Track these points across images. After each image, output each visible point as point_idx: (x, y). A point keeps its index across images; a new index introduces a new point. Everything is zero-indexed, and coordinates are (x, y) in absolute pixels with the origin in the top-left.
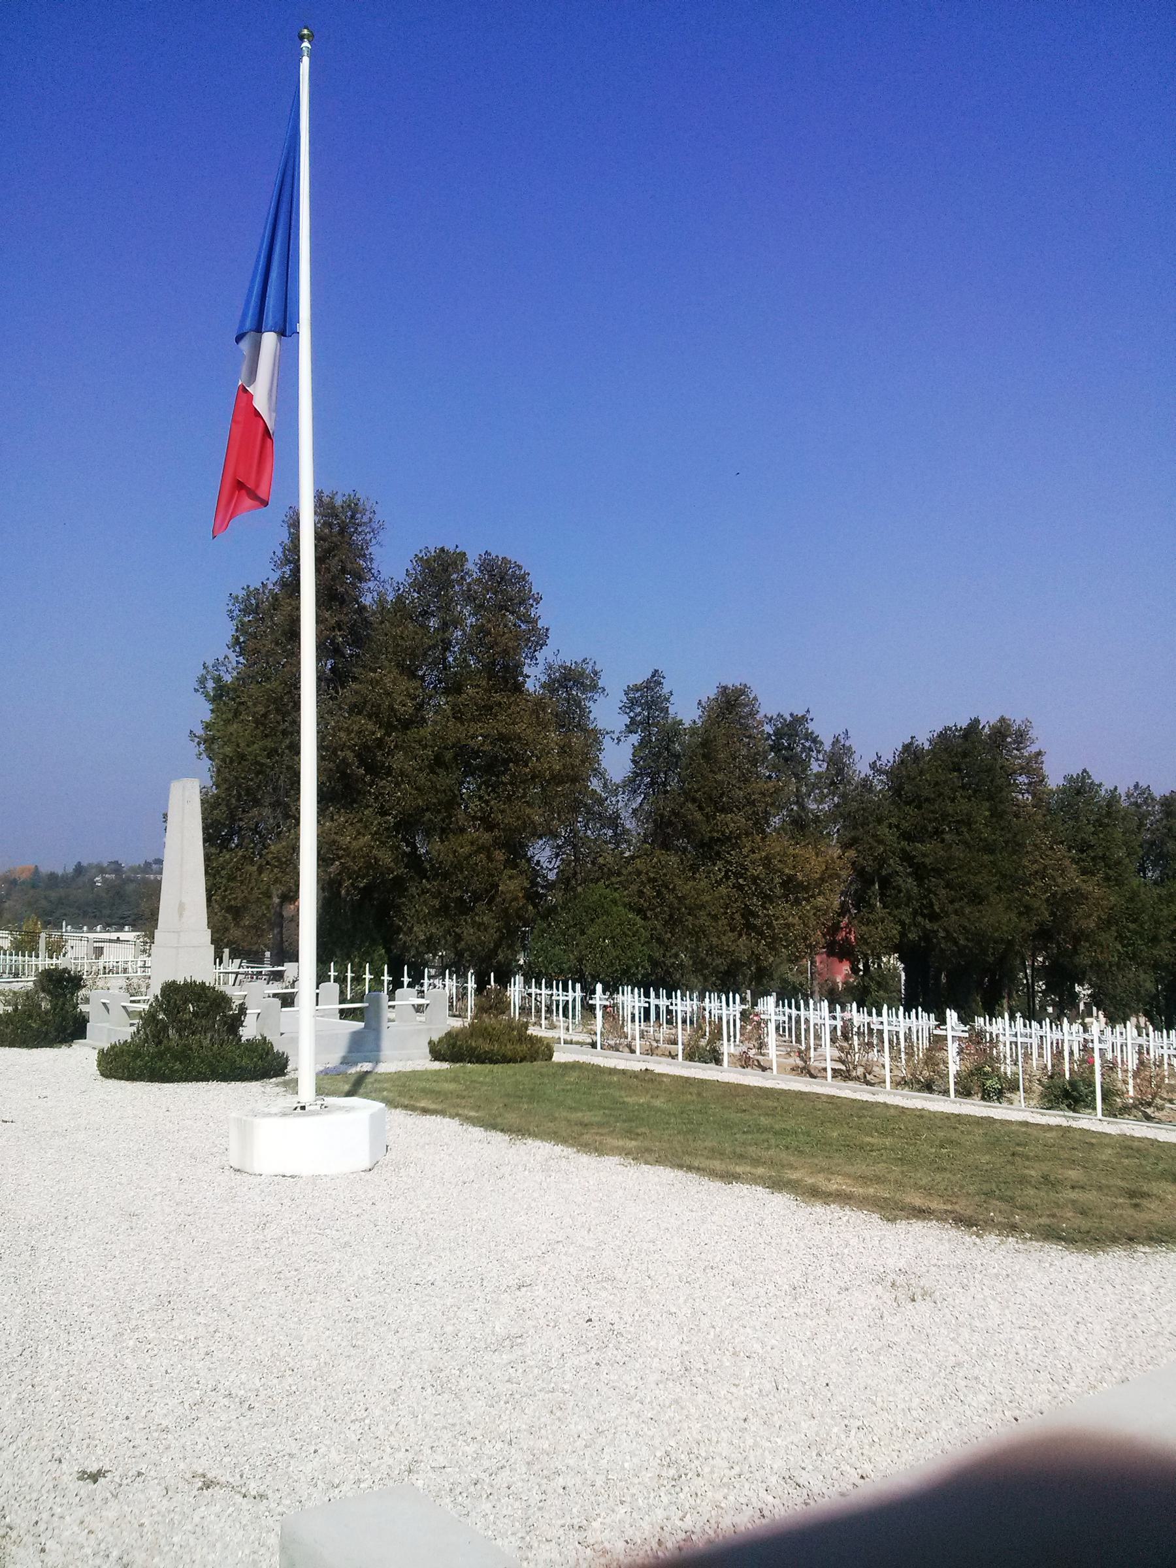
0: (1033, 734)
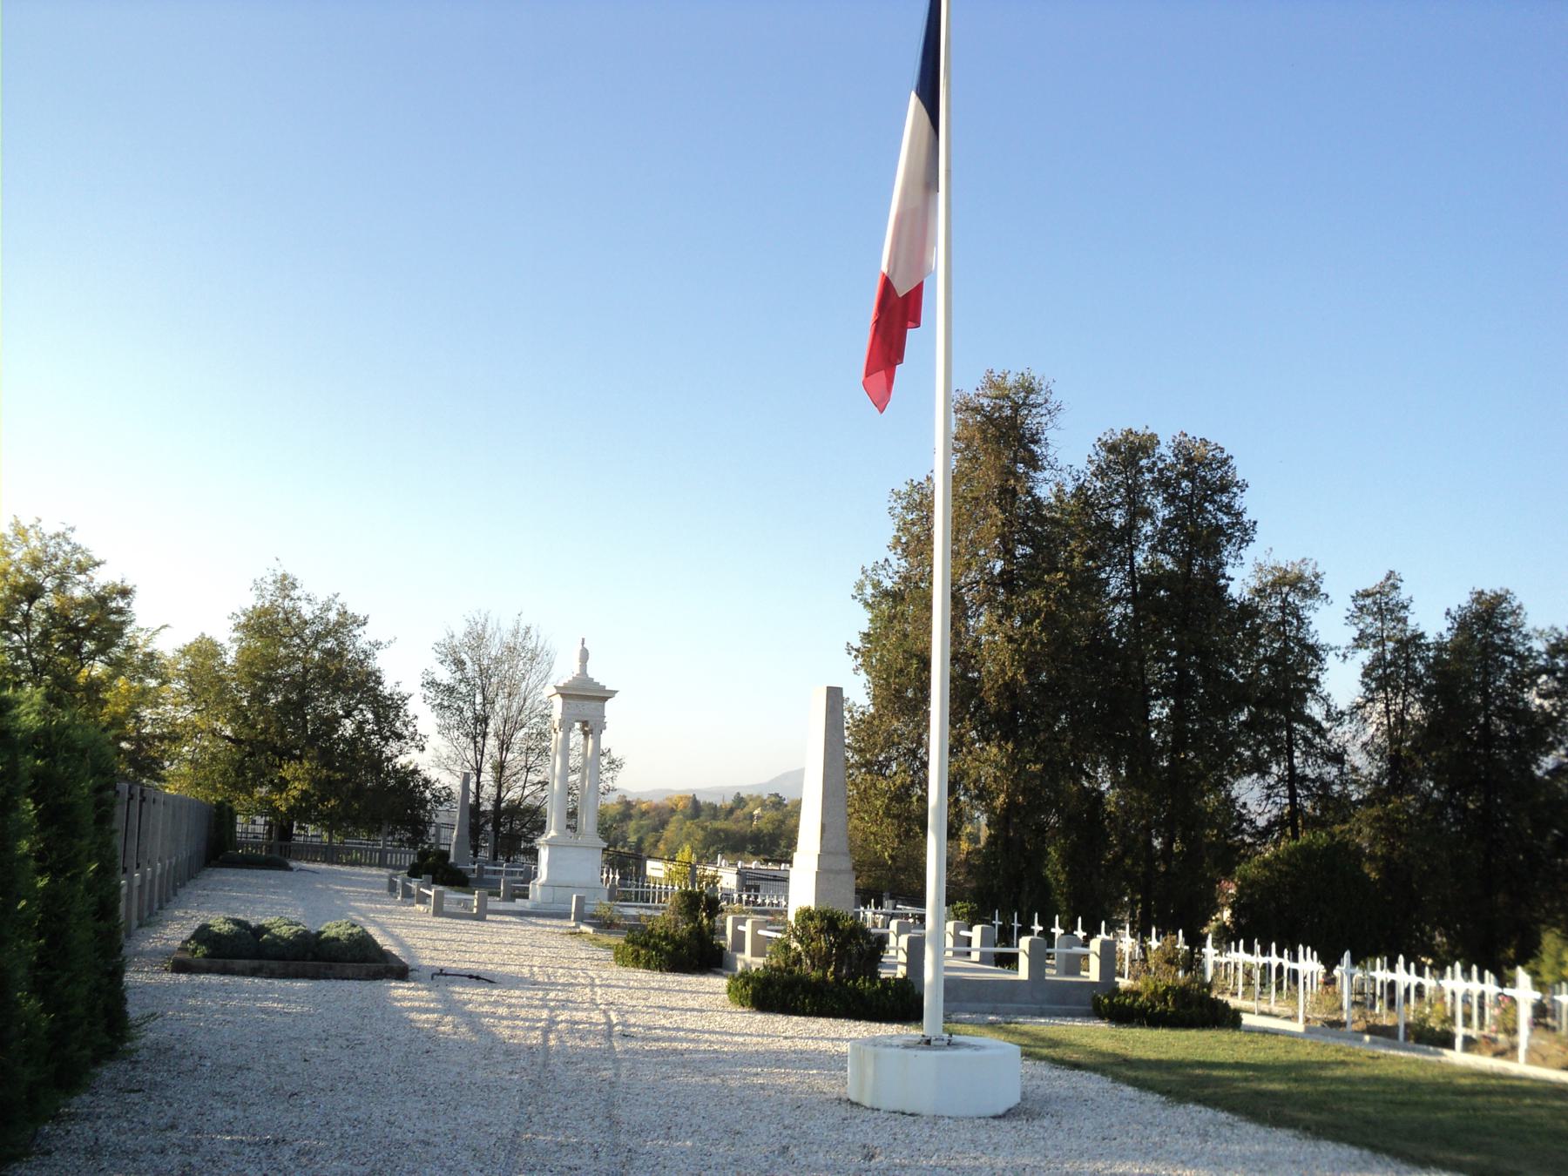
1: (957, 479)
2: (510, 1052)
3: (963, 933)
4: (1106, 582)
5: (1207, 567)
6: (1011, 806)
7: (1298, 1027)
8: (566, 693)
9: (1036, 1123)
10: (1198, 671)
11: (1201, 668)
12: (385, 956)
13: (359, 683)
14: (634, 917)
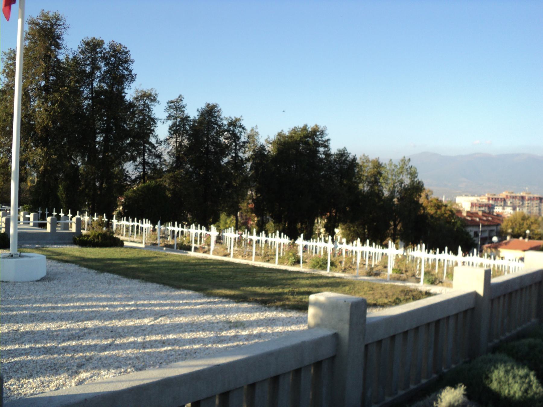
0: (327, 132)
4: (83, 92)
5: (118, 89)
6: (45, 170)
7: (143, 246)
9: (52, 282)
11: (114, 124)
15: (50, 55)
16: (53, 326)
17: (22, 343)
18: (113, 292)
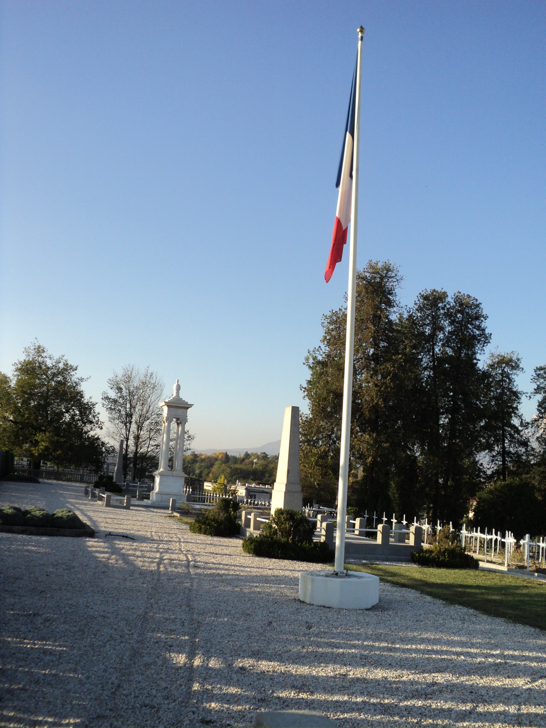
1: (357, 310)
2: (143, 574)
3: (351, 521)
4: (421, 360)
5: (468, 354)
6: (374, 462)
7: (504, 568)
8: (170, 405)
9: (386, 613)
10: (462, 402)
11: (463, 401)
12: (84, 525)
13: (74, 397)
14: (199, 510)
15: (380, 315)
16: (391, 675)
17: (353, 694)
18: (469, 634)
